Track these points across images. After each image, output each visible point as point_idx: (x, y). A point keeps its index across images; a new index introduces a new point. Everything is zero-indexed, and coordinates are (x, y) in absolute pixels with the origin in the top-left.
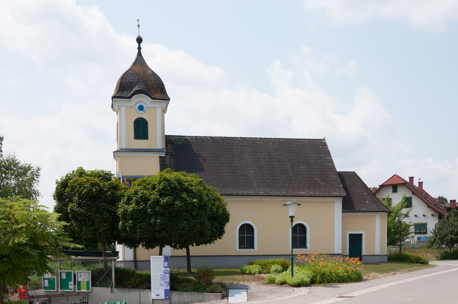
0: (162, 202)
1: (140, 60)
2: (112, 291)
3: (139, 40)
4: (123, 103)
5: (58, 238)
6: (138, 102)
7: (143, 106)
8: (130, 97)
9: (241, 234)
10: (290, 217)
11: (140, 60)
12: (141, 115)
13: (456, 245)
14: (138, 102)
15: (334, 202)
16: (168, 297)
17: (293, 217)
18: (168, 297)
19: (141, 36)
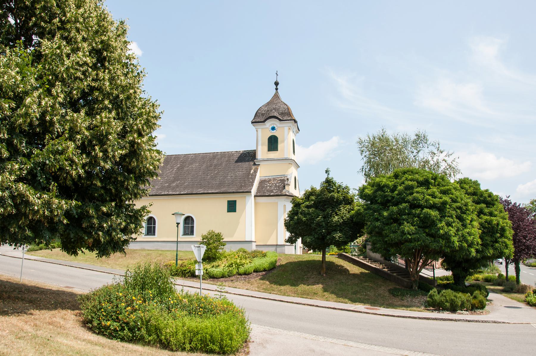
0: (36, 172)
1: (276, 96)
2: (52, 250)
3: (277, 84)
4: (260, 126)
5: (29, 197)
6: (273, 124)
7: (274, 127)
8: (264, 122)
9: (151, 231)
10: (177, 223)
11: (276, 96)
12: (274, 133)
13: (100, 65)
14: (273, 124)
15: (245, 197)
16: (411, 269)
17: (179, 223)
18: (411, 269)
19: (278, 81)
